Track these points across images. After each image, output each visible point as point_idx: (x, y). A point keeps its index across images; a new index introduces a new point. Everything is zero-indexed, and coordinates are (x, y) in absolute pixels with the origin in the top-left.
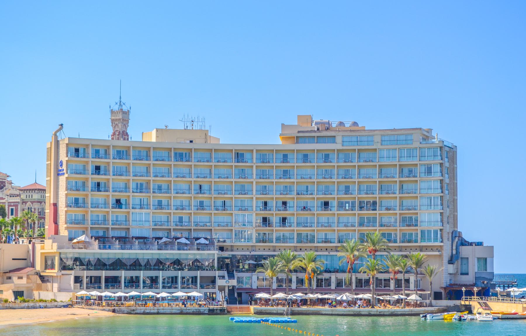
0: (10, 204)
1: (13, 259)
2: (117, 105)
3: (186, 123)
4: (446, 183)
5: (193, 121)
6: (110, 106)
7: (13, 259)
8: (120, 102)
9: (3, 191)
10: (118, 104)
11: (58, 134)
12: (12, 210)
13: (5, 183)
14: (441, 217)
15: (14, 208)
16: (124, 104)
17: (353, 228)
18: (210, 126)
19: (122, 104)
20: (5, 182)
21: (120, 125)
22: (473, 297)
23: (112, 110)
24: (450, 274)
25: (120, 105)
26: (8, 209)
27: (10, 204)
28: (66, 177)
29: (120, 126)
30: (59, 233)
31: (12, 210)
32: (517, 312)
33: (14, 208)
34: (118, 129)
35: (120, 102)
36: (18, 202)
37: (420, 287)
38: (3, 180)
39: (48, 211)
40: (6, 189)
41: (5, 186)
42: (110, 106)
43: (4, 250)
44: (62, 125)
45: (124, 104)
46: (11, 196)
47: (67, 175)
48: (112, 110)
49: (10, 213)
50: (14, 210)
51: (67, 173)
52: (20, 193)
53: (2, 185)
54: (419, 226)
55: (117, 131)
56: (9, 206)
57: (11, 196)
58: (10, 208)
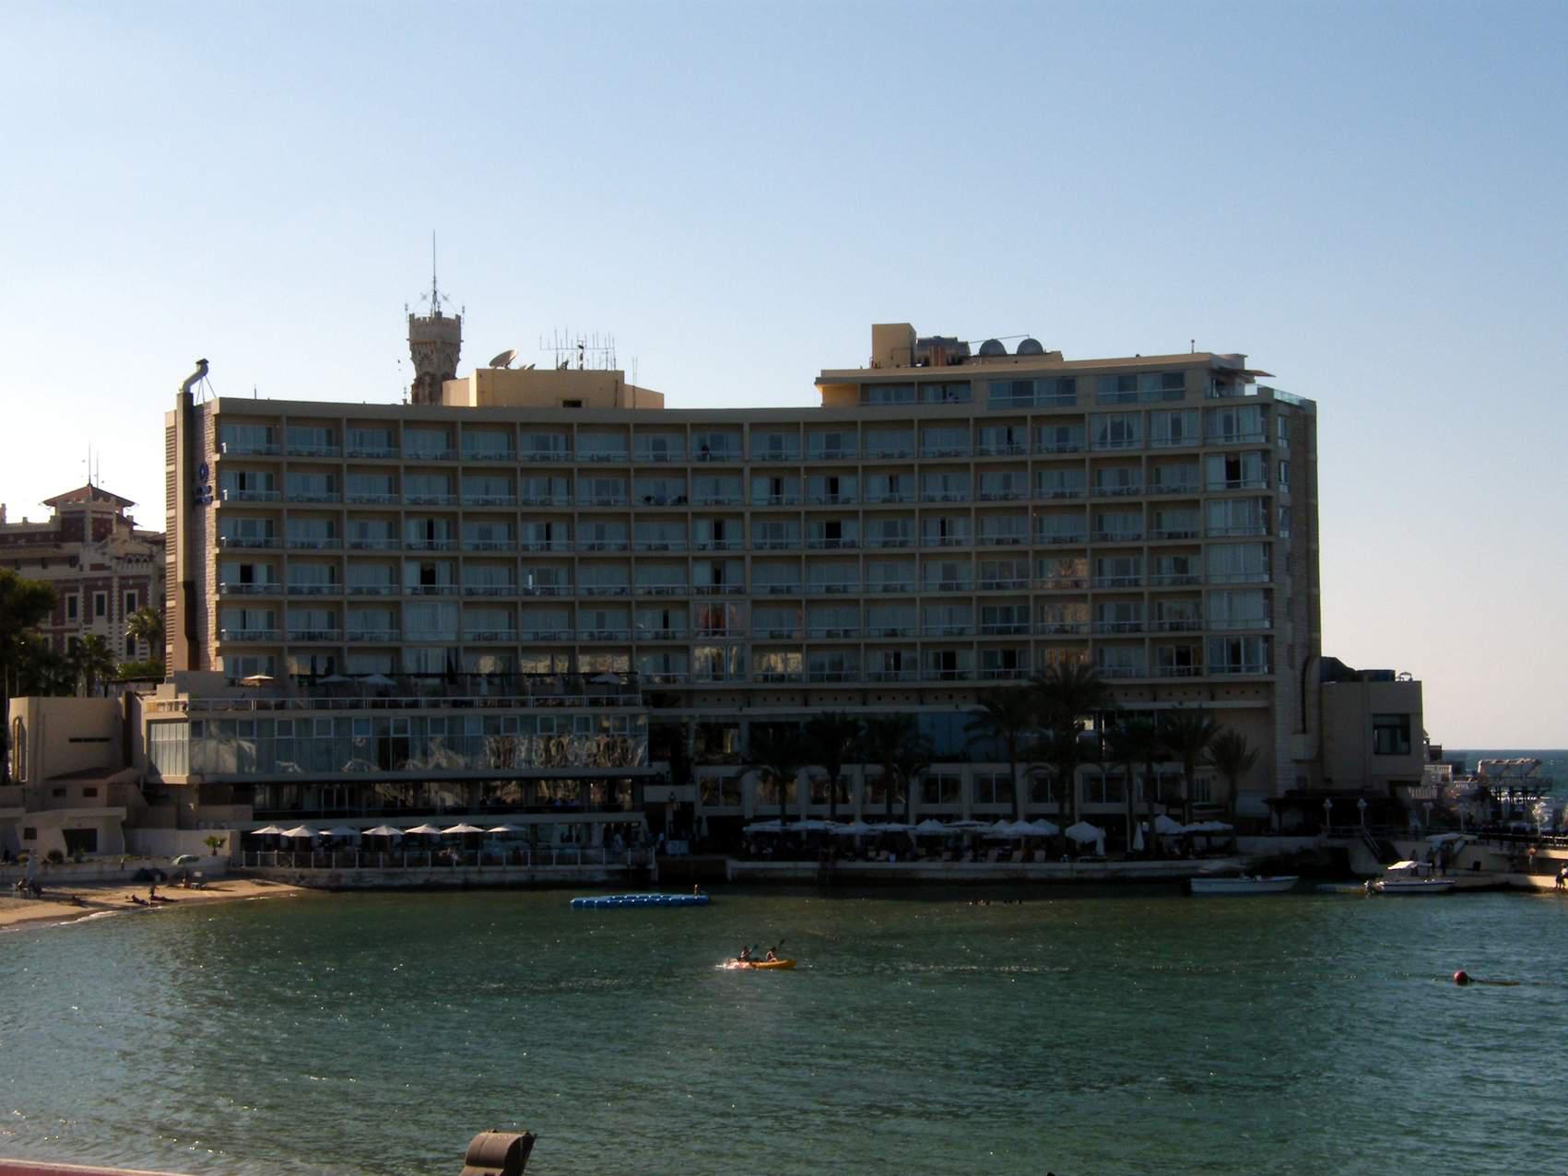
0: (123, 582)
1: (72, 740)
2: (425, 302)
3: (560, 351)
4: (1282, 506)
5: (581, 347)
6: (406, 305)
7: (72, 740)
8: (435, 292)
9: (105, 545)
10: (430, 298)
11: (194, 389)
12: (131, 597)
13: (111, 525)
14: (1267, 602)
15: (136, 592)
16: (445, 298)
17: (1138, 635)
18: (635, 360)
19: (439, 298)
20: (110, 521)
21: (434, 357)
22: (1355, 827)
23: (412, 316)
24: (1298, 762)
25: (435, 300)
26: (121, 597)
27: (123, 582)
28: (217, 509)
29: (435, 360)
30: (201, 665)
31: (131, 597)
32: (198, 855)
33: (105, 593)
34: (430, 370)
35: (435, 292)
36: (147, 577)
37: (1209, 800)
38: (105, 516)
39: (175, 603)
40: (113, 540)
41: (110, 531)
42: (406, 305)
43: (44, 717)
44: (203, 364)
45: (445, 298)
46: (129, 559)
47: (219, 502)
48: (412, 316)
49: (95, 609)
50: (137, 598)
51: (220, 496)
52: (151, 551)
53: (102, 530)
54: (1032, 631)
55: (427, 373)
56: (122, 588)
57: (130, 561)
58: (126, 592)
